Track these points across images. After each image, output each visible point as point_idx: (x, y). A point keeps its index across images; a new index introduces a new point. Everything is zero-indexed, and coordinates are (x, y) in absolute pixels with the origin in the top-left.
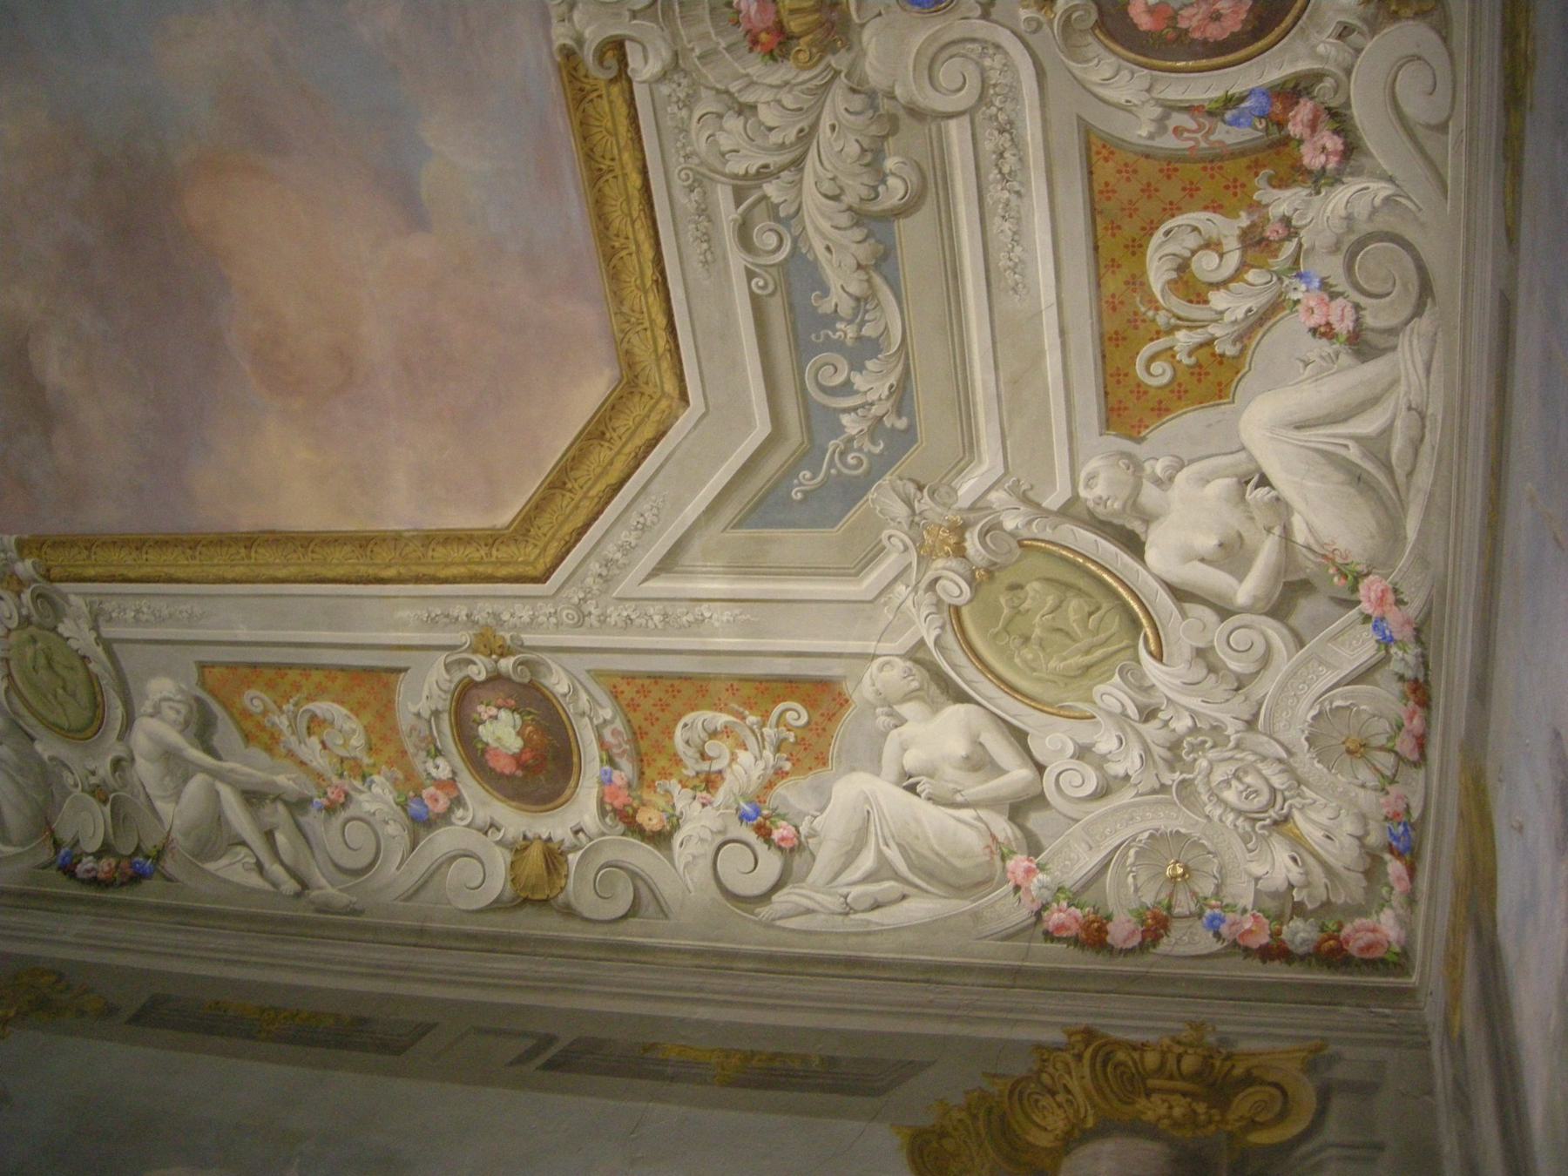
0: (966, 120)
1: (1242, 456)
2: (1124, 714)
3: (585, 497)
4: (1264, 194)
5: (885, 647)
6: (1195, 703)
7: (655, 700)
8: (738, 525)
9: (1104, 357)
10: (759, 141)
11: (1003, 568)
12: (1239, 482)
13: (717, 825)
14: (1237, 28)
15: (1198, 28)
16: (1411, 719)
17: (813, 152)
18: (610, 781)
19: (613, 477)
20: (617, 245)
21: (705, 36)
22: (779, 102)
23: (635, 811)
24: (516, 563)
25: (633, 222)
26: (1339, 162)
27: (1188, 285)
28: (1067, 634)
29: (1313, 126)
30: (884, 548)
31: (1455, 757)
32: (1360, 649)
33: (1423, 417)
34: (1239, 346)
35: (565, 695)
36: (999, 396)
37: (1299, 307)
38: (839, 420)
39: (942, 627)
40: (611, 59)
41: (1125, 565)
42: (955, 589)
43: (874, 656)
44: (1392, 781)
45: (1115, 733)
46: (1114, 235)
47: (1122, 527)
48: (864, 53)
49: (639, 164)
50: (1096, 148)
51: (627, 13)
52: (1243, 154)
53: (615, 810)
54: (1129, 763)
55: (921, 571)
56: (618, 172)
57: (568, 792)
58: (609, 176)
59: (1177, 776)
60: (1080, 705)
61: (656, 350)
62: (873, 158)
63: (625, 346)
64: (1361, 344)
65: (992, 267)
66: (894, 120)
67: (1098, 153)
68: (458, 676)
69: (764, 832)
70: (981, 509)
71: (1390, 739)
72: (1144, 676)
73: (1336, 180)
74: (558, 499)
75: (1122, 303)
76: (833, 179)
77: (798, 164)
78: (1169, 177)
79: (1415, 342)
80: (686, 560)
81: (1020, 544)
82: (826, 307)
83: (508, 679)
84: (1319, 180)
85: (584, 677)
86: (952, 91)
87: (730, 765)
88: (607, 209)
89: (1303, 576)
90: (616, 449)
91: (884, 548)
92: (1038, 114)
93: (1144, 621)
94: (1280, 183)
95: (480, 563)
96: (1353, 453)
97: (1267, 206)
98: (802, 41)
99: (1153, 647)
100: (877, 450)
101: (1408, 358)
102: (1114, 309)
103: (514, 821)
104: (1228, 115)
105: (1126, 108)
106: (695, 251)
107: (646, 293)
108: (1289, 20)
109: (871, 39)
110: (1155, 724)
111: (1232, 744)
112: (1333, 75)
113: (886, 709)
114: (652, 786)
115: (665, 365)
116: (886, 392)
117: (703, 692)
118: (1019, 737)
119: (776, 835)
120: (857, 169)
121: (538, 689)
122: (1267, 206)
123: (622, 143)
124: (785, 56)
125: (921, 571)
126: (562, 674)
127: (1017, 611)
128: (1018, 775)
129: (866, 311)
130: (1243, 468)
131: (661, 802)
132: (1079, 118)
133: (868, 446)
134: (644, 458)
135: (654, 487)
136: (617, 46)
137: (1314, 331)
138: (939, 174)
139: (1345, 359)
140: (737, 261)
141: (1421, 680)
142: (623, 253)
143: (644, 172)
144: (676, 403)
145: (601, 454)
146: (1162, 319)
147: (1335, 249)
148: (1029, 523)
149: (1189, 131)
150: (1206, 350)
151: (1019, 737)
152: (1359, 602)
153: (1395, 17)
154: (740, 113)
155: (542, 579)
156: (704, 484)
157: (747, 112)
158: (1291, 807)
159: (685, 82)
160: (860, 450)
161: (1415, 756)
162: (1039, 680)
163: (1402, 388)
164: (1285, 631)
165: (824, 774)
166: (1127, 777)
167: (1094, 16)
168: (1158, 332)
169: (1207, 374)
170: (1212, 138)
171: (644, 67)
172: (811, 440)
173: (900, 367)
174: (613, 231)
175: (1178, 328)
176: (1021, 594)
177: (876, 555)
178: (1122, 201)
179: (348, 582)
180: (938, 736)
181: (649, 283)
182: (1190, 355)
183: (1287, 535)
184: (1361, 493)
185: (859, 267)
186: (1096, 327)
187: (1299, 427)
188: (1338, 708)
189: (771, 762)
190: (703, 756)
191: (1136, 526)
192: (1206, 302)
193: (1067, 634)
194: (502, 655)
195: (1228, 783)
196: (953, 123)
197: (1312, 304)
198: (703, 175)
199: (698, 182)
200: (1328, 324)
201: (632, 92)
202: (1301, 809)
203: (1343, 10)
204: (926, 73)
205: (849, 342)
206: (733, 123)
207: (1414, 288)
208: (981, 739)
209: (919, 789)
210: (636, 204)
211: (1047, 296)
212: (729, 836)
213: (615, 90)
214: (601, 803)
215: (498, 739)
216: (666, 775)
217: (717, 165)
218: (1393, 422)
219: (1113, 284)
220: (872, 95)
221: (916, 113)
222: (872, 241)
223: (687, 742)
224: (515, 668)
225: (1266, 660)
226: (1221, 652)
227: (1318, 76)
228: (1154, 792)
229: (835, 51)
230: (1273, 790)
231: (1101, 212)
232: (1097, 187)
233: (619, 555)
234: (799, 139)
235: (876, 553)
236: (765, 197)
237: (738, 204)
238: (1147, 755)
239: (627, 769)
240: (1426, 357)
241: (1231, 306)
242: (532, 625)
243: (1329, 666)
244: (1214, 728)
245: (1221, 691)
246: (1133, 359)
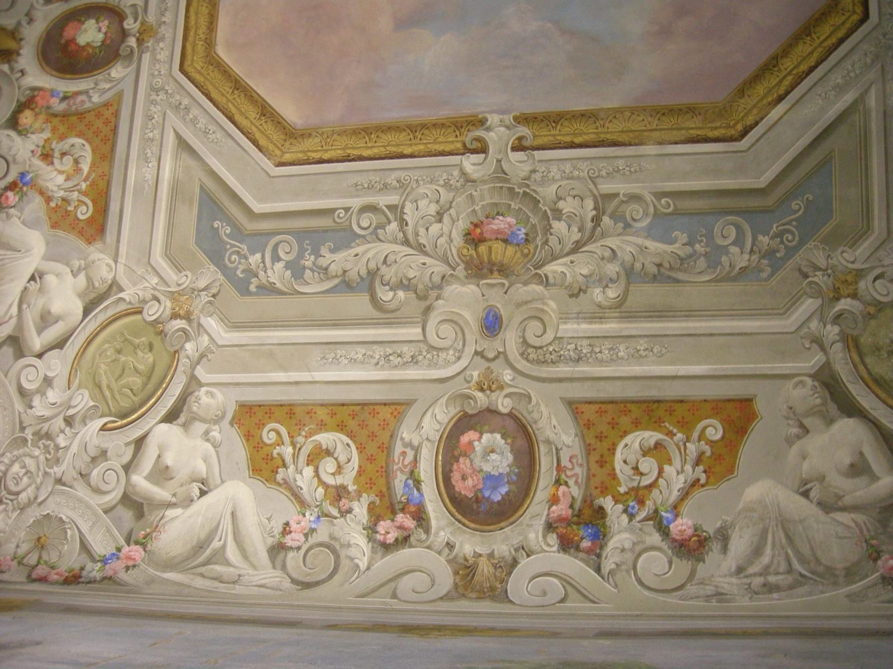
0: (422, 338)
1: (219, 481)
2: (69, 407)
3: (228, 100)
4: (365, 499)
5: (121, 268)
6: (74, 448)
7: (102, 129)
8: (202, 188)
9: (281, 406)
10: (421, 222)
11: (163, 340)
12: (203, 479)
13: (19, 158)
14: (457, 489)
15: (459, 468)
16: (57, 574)
17: (412, 252)
18: (53, 96)
19: (238, 117)
20: (373, 136)
21: (482, 198)
22: (441, 236)
23: (32, 109)
24: (193, 56)
25: (384, 146)
26: (380, 541)
27: (318, 455)
28: (121, 376)
29: (401, 527)
30: (180, 272)
31: (33, 597)
32: (101, 546)
33: (234, 583)
34: (281, 482)
35: (109, 74)
36: (263, 345)
37: (301, 516)
38: (258, 252)
39: (130, 303)
40: (476, 145)
41: (159, 412)
42: (152, 312)
43: (116, 262)
44: (19, 563)
45: (59, 401)
46: (349, 415)
47: (181, 411)
48: (464, 284)
49: (416, 153)
50: (399, 408)
52: (389, 488)
53: (33, 97)
54: (40, 408)
55: (164, 293)
56: (413, 142)
57: (48, 69)
58: (411, 136)
59: (30, 437)
60: (77, 381)
61: (309, 151)
62: (405, 284)
63: (314, 134)
64: (278, 550)
65: (338, 346)
66: (424, 298)
67: (396, 409)
68: (128, 11)
69: (12, 186)
70: (199, 329)
71: (46, 562)
72: (92, 419)
73: (370, 539)
74: (229, 85)
75: (311, 417)
76: (396, 261)
77: (406, 242)
78: (379, 447)
79: (277, 579)
80: (185, 156)
81: (176, 352)
82: (324, 251)
83: (123, 41)
84: (371, 530)
85: (120, 87)
86: (439, 332)
87: (56, 170)
88: (393, 133)
89: (146, 514)
90: (254, 121)
91: (180, 272)
92: (420, 377)
93: (125, 421)
94: (371, 508)
95: (195, 33)
96: (216, 544)
97: (359, 501)
98: (473, 252)
99: (109, 425)
100: (238, 272)
101: (269, 575)
102: (308, 413)
103: (33, 34)
104: (410, 482)
105: (419, 426)
106: (363, 180)
107: (344, 149)
108: (460, 517)
109: (471, 289)
110: (63, 425)
111: (48, 470)
112: (427, 539)
113: (83, 266)
114: (47, 121)
115: (300, 156)
116: (271, 280)
117: (103, 158)
118: (60, 344)
119: (10, 194)
120: (400, 275)
121: (115, 58)
122: (359, 501)
123: (429, 146)
124: (466, 242)
125: (164, 293)
126: (122, 75)
127: (136, 347)
128: (37, 342)
129: (319, 273)
130: (211, 481)
131: (37, 125)
132: (416, 400)
133: (241, 267)
134: (248, 138)
135: (230, 143)
136: (482, 149)
137: (287, 524)
138: (393, 320)
139: (270, 541)
140: (356, 203)
141: (81, 580)
142: (367, 139)
143: (412, 156)
144: (278, 160)
145: (252, 113)
146: (300, 439)
147: (332, 537)
148: (188, 357)
149: (403, 460)
150: (281, 463)
151: (60, 344)
152: (129, 545)
153: (456, 573)
154: (438, 213)
155: (182, 69)
156: (228, 171)
157: (438, 217)
158: (7, 504)
159: (459, 184)
160: (240, 263)
161: (34, 576)
162: (94, 358)
163: (251, 572)
164: (114, 503)
165: (47, 227)
166: (31, 407)
167: (470, 412)
168: (292, 437)
169: (267, 463)
170: (398, 473)
171: (469, 163)
172: (248, 235)
173: (285, 290)
174: (381, 135)
175: (294, 448)
176: (146, 350)
177: (176, 267)
178: (368, 421)
180: (64, 297)
181: (349, 151)
182: (278, 454)
183: (170, 505)
184: (193, 548)
185: (345, 272)
186: (299, 402)
187: (233, 514)
188: (66, 532)
189: (56, 195)
190: (63, 154)
191: (182, 419)
192: (308, 465)
193: (121, 376)
194: (138, 40)
195: (24, 467)
196: (419, 330)
197: (302, 524)
198: (406, 189)
199: (402, 185)
200: (291, 532)
201: (456, 154)
202: (5, 510)
203: (461, 546)
204: (448, 318)
205: (303, 262)
206: (433, 209)
207: (307, 579)
208: (60, 322)
209: (32, 282)
210: (394, 149)
211: (319, 376)
212: (12, 166)
213: (459, 145)
214: (40, 89)
215: (86, 31)
216: (54, 130)
217: (411, 197)
218: (233, 566)
219: (322, 413)
220: (440, 287)
221: (428, 310)
222: (359, 280)
223: (73, 145)
224: (128, 46)
225: (98, 491)
226: (104, 465)
227: (427, 531)
228: (21, 423)
229: (466, 269)
230: (17, 494)
231: (363, 409)
232: (376, 407)
233: (191, 116)
234: (420, 244)
235: (178, 268)
236: (389, 222)
237: (388, 207)
238: (43, 419)
239: (59, 107)
240: (268, 585)
241: (305, 478)
242: (154, 60)
243: (92, 527)
244: (58, 460)
245: (80, 465)
246: (279, 422)
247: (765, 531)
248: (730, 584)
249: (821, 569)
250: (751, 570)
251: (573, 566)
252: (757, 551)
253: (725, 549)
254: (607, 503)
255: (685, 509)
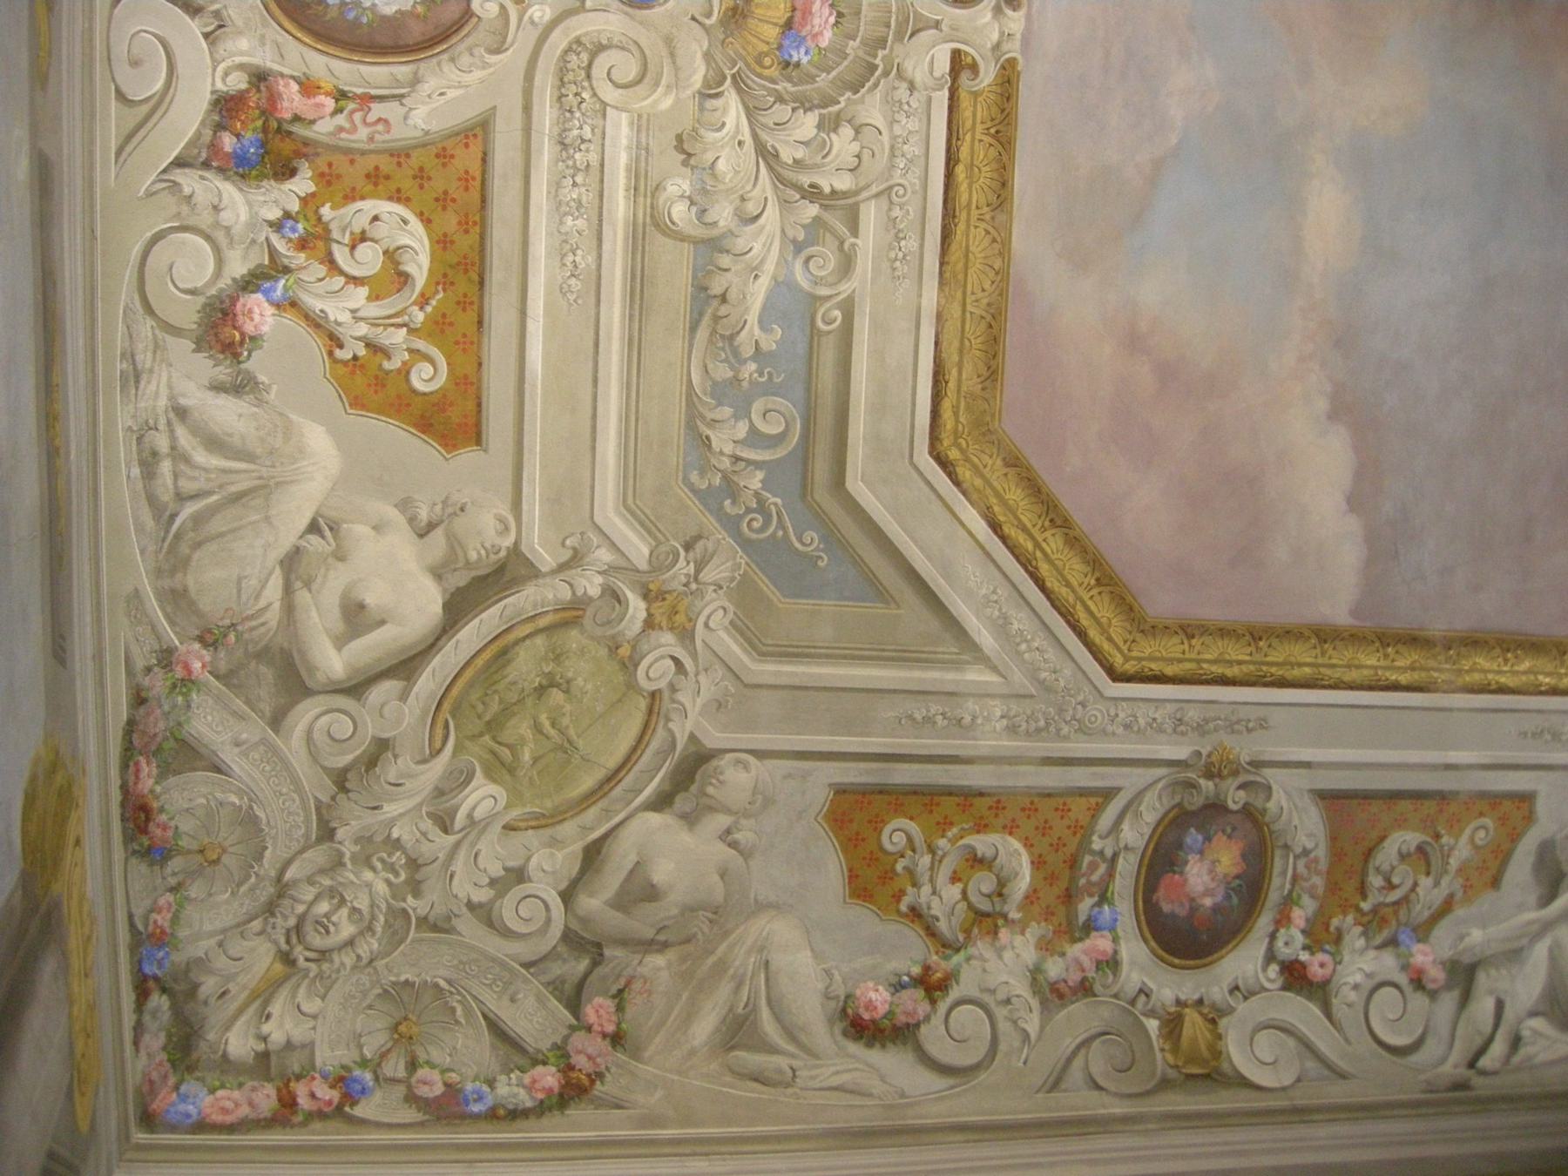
51: (944, 27)
179: (1371, 688)
188: (248, 877)
204: (647, 52)
223: (376, 218)
247: (249, 457)
248: (155, 394)
249: (184, 549)
250: (181, 431)
252: (214, 443)
253: (218, 388)
254: (302, 184)
255: (290, 321)
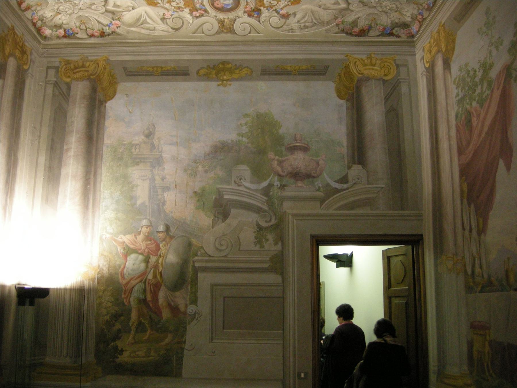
94: (190, 10)
96: (142, 19)
101: (162, 27)
153: (219, 23)
183: (123, 12)
207: (176, 27)
247: (306, 14)
248: (295, 26)
249: (320, 21)
250: (301, 22)
251: (252, 21)
252: (304, 17)
253: (295, 17)
254: (262, 8)
255: (284, 9)
